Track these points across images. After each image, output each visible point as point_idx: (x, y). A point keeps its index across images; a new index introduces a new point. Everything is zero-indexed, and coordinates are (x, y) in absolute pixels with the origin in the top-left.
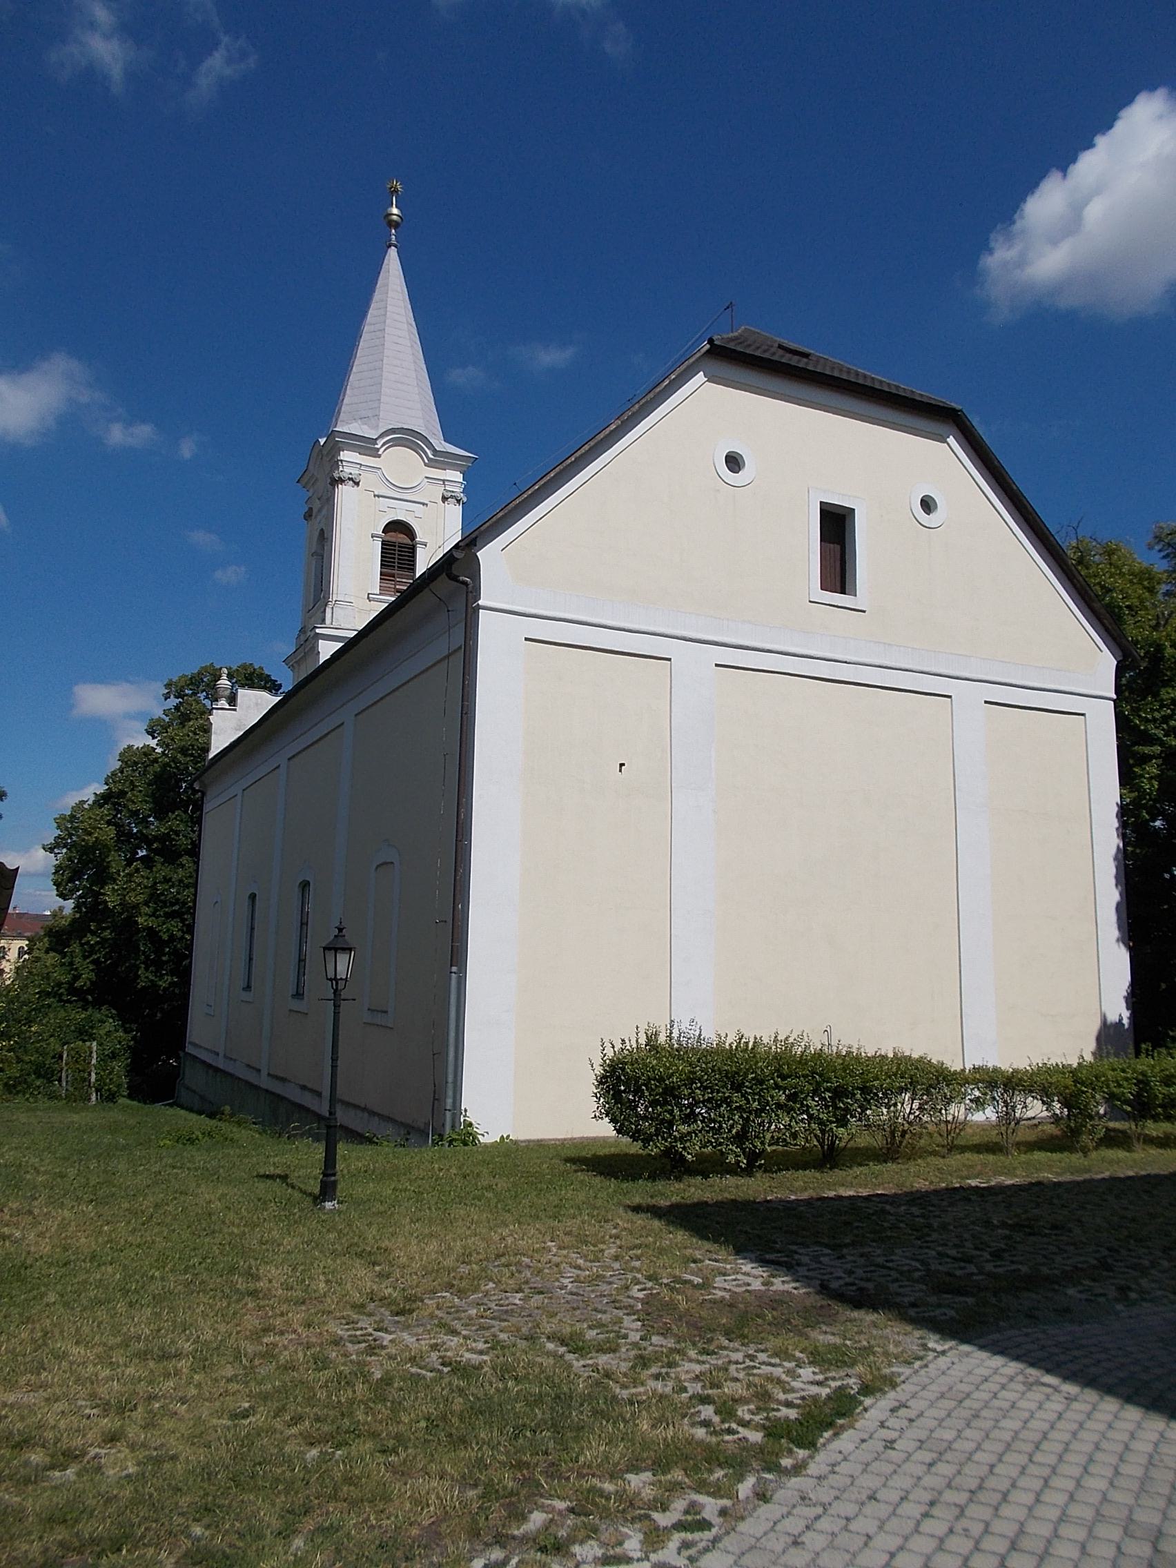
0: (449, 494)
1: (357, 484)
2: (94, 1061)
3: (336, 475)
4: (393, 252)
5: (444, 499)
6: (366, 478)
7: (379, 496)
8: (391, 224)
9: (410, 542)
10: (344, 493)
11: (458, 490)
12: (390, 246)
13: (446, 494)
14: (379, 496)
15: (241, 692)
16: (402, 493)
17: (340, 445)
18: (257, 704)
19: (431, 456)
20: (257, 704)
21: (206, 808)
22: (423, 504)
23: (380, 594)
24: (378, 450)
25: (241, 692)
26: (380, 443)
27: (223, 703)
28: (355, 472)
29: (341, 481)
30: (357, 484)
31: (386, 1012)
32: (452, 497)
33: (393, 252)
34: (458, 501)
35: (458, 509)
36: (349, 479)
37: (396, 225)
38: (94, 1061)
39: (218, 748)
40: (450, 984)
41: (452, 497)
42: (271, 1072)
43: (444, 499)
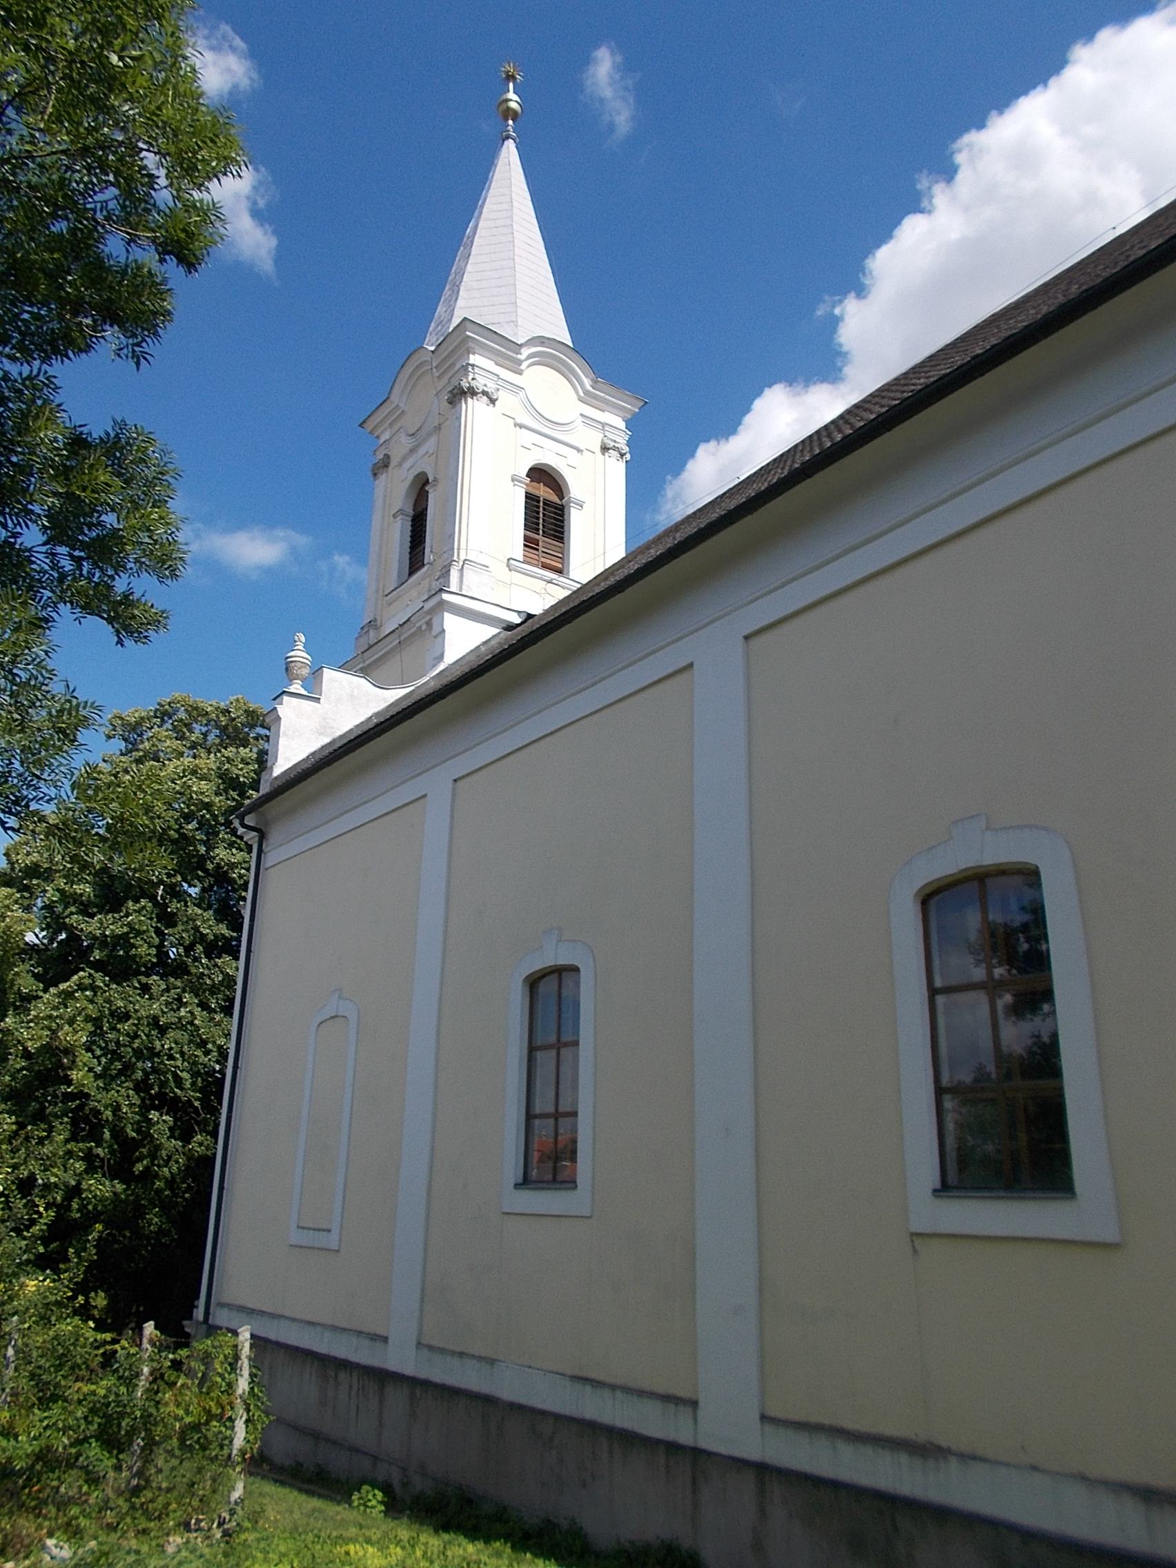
0: (612, 444)
1: (493, 401)
2: (243, 1385)
3: (465, 384)
4: (510, 151)
5: (605, 449)
6: (503, 397)
7: (521, 426)
8: (508, 113)
9: (559, 502)
10: (474, 409)
11: (622, 441)
12: (508, 137)
13: (606, 440)
14: (521, 426)
15: (329, 675)
16: (549, 428)
17: (470, 344)
18: (352, 697)
19: (590, 388)
20: (352, 697)
21: (270, 859)
22: (579, 450)
23: (524, 562)
24: (520, 362)
25: (329, 675)
26: (525, 352)
27: (296, 687)
28: (491, 387)
29: (472, 392)
30: (493, 401)
31: (329, 1231)
32: (614, 448)
33: (510, 151)
34: (622, 455)
35: (621, 466)
36: (485, 393)
37: (515, 115)
38: (243, 1385)
39: (289, 760)
40: (211, 1193)
41: (614, 448)
42: (773, 1412)
43: (605, 449)
